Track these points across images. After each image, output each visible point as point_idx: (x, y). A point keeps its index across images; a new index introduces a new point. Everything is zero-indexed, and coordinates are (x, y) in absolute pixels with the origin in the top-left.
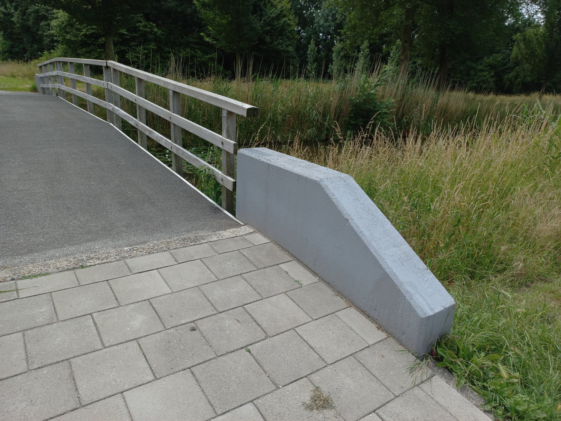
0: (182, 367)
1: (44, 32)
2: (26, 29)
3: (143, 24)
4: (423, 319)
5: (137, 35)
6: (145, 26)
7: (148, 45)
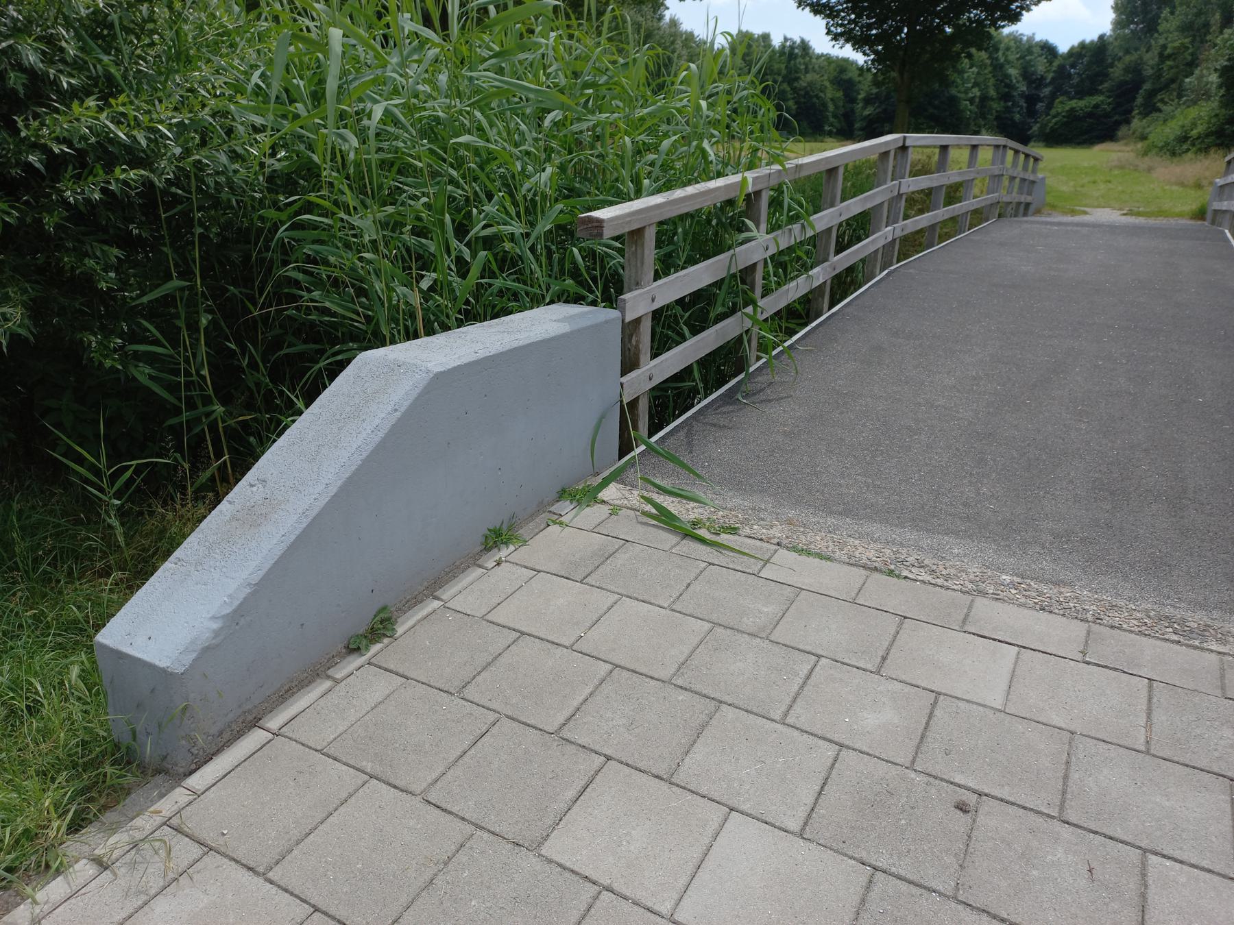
0: (864, 856)
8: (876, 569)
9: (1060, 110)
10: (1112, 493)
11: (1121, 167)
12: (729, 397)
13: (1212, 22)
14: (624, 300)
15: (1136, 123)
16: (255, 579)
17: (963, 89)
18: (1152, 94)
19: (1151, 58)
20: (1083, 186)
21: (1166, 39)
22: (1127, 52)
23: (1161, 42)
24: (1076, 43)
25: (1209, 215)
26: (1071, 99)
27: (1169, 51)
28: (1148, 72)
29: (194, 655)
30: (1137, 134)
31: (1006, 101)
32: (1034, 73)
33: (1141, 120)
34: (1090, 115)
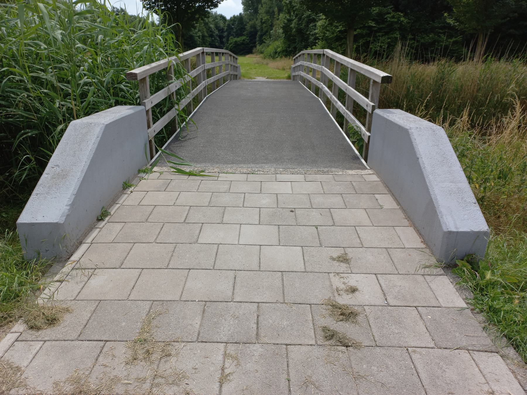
0: (275, 224)
1: (311, 31)
2: (300, 31)
3: (392, 15)
4: (445, 232)
5: (384, 26)
6: (393, 17)
7: (392, 34)
8: (248, 173)
9: (232, 41)
10: (298, 148)
11: (258, 63)
12: (176, 139)
13: (275, 11)
14: (145, 103)
15: (258, 47)
16: (75, 192)
17: (195, 32)
18: (261, 36)
19: (258, 23)
20: (248, 70)
21: (262, 16)
22: (250, 20)
23: (261, 17)
24: (232, 16)
25: (292, 77)
26: (235, 37)
27: (263, 21)
28: (258, 28)
29: (65, 217)
30: (259, 51)
31: (212, 38)
32: (220, 27)
33: (259, 46)
34: (243, 44)
